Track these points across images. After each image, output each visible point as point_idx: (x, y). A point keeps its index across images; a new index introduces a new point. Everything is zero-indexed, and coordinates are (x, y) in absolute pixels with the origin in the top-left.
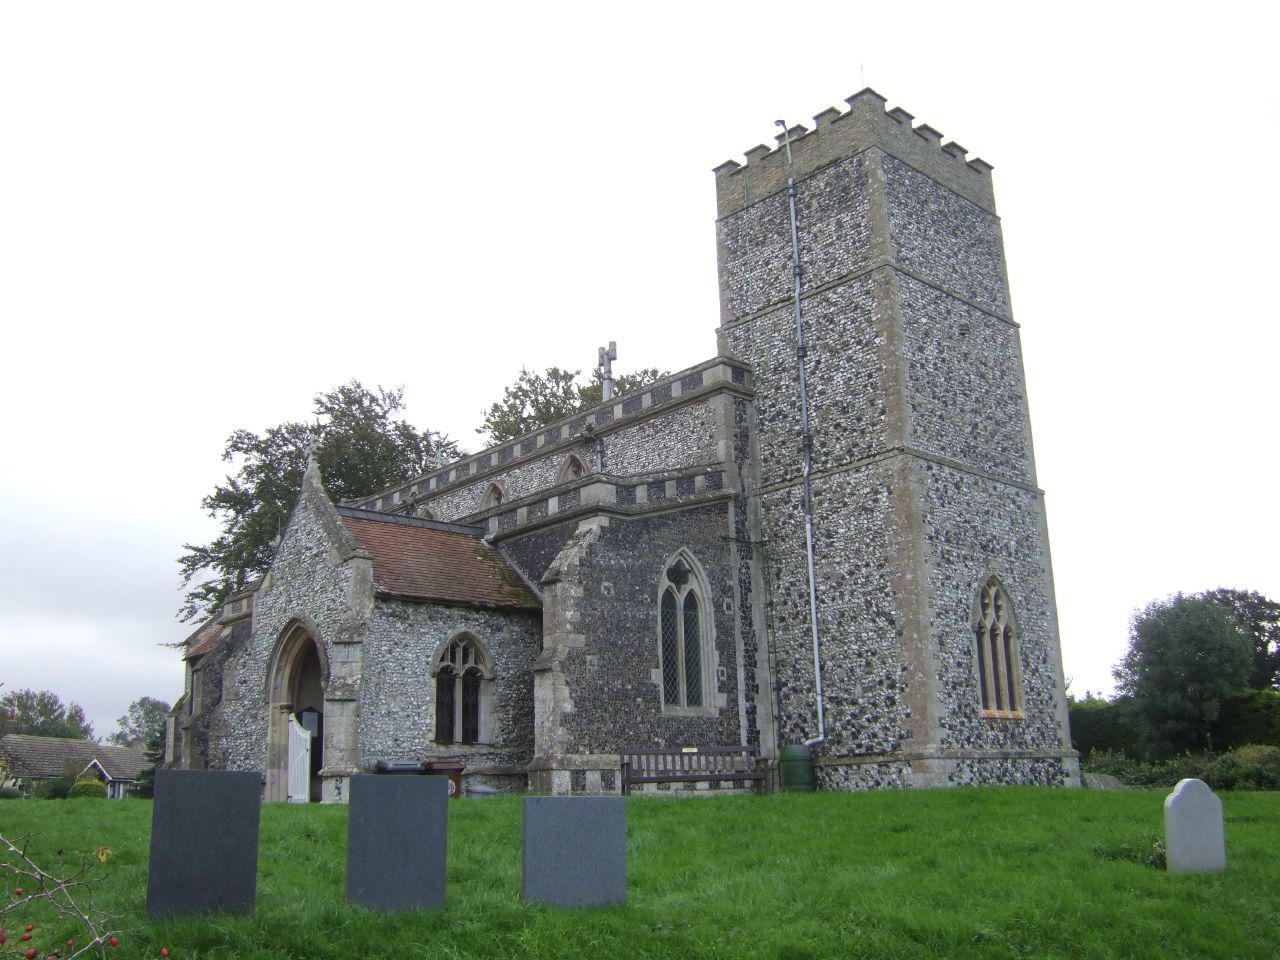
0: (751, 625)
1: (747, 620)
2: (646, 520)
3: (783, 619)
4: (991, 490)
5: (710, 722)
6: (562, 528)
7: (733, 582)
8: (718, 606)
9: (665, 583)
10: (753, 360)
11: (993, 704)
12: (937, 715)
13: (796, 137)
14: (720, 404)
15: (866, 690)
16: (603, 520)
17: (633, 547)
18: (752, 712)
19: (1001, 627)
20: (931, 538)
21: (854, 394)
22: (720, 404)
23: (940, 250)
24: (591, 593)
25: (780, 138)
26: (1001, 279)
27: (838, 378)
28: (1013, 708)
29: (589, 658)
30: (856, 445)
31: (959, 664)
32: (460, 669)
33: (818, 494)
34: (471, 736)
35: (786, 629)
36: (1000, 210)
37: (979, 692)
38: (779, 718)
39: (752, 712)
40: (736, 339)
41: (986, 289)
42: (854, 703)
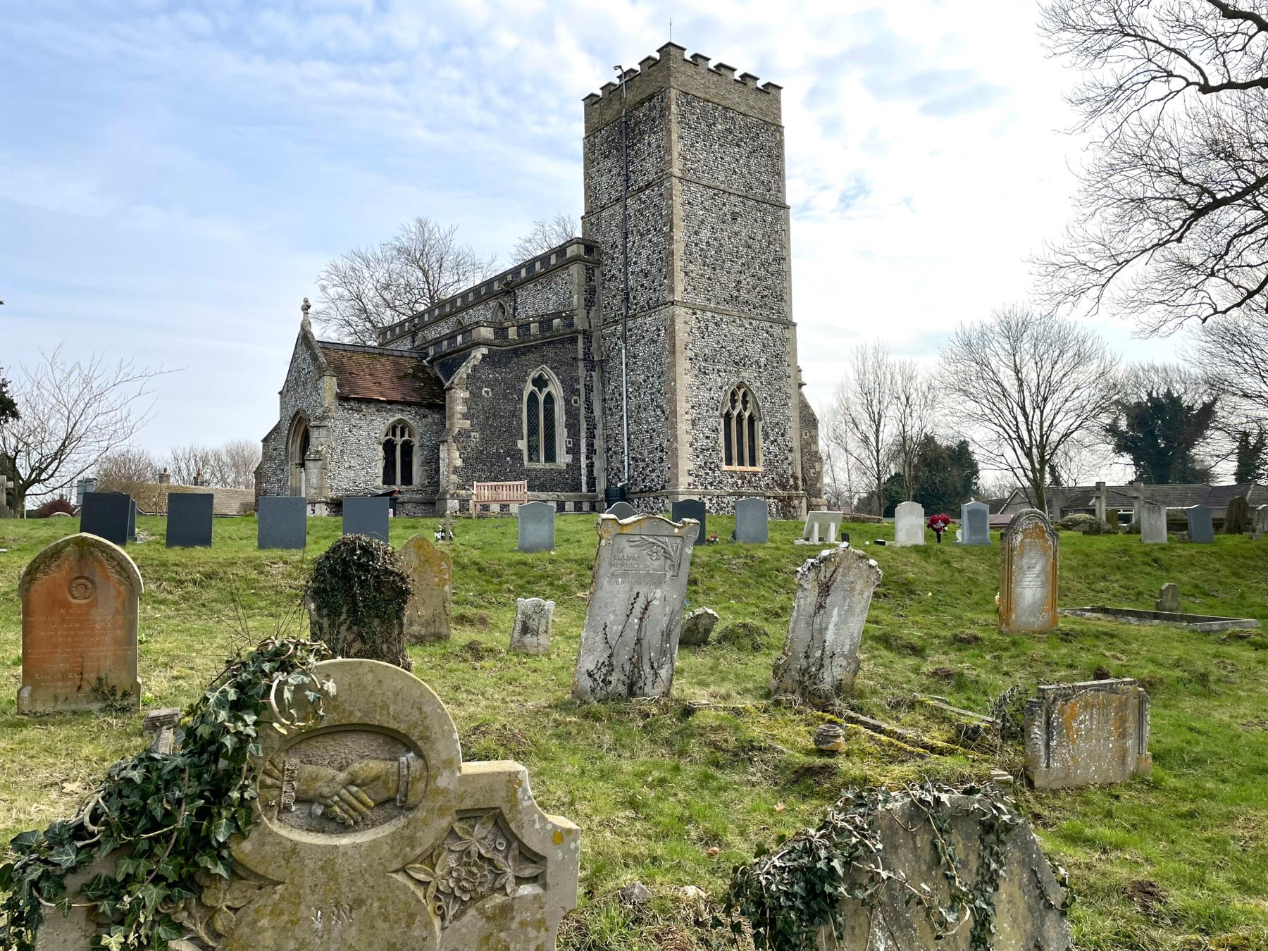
0: (592, 413)
1: (589, 408)
2: (515, 349)
3: (610, 409)
4: (747, 326)
5: (560, 472)
6: (462, 354)
7: (581, 387)
8: (567, 402)
9: (529, 387)
10: (600, 239)
11: (735, 461)
12: (686, 468)
13: (629, 76)
14: (576, 270)
15: (650, 453)
16: (485, 350)
17: (505, 366)
18: (590, 467)
19: (747, 414)
20: (691, 359)
21: (652, 264)
22: (576, 270)
23: (722, 158)
24: (475, 395)
25: (620, 77)
26: (779, 174)
27: (644, 253)
28: (753, 463)
29: (473, 434)
30: (651, 299)
31: (707, 438)
32: (399, 440)
33: (630, 330)
34: (407, 479)
35: (612, 415)
36: (784, 121)
37: (723, 454)
38: (607, 469)
39: (590, 467)
40: (592, 224)
41: (763, 182)
42: (644, 461)
